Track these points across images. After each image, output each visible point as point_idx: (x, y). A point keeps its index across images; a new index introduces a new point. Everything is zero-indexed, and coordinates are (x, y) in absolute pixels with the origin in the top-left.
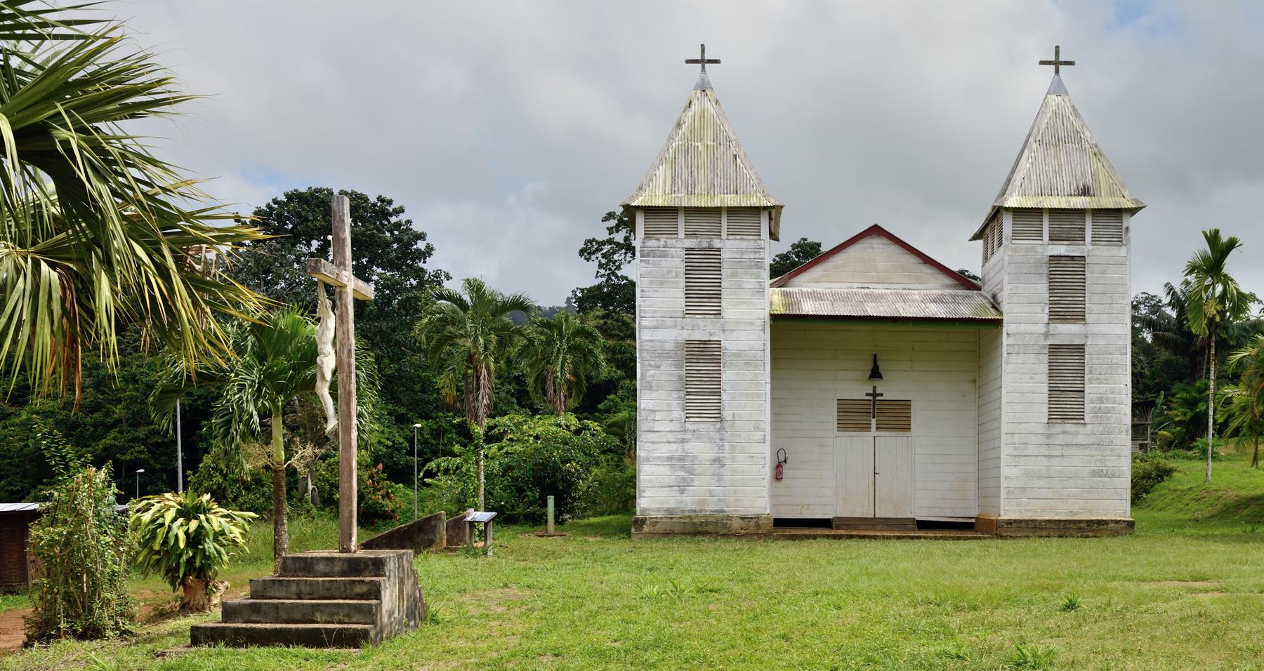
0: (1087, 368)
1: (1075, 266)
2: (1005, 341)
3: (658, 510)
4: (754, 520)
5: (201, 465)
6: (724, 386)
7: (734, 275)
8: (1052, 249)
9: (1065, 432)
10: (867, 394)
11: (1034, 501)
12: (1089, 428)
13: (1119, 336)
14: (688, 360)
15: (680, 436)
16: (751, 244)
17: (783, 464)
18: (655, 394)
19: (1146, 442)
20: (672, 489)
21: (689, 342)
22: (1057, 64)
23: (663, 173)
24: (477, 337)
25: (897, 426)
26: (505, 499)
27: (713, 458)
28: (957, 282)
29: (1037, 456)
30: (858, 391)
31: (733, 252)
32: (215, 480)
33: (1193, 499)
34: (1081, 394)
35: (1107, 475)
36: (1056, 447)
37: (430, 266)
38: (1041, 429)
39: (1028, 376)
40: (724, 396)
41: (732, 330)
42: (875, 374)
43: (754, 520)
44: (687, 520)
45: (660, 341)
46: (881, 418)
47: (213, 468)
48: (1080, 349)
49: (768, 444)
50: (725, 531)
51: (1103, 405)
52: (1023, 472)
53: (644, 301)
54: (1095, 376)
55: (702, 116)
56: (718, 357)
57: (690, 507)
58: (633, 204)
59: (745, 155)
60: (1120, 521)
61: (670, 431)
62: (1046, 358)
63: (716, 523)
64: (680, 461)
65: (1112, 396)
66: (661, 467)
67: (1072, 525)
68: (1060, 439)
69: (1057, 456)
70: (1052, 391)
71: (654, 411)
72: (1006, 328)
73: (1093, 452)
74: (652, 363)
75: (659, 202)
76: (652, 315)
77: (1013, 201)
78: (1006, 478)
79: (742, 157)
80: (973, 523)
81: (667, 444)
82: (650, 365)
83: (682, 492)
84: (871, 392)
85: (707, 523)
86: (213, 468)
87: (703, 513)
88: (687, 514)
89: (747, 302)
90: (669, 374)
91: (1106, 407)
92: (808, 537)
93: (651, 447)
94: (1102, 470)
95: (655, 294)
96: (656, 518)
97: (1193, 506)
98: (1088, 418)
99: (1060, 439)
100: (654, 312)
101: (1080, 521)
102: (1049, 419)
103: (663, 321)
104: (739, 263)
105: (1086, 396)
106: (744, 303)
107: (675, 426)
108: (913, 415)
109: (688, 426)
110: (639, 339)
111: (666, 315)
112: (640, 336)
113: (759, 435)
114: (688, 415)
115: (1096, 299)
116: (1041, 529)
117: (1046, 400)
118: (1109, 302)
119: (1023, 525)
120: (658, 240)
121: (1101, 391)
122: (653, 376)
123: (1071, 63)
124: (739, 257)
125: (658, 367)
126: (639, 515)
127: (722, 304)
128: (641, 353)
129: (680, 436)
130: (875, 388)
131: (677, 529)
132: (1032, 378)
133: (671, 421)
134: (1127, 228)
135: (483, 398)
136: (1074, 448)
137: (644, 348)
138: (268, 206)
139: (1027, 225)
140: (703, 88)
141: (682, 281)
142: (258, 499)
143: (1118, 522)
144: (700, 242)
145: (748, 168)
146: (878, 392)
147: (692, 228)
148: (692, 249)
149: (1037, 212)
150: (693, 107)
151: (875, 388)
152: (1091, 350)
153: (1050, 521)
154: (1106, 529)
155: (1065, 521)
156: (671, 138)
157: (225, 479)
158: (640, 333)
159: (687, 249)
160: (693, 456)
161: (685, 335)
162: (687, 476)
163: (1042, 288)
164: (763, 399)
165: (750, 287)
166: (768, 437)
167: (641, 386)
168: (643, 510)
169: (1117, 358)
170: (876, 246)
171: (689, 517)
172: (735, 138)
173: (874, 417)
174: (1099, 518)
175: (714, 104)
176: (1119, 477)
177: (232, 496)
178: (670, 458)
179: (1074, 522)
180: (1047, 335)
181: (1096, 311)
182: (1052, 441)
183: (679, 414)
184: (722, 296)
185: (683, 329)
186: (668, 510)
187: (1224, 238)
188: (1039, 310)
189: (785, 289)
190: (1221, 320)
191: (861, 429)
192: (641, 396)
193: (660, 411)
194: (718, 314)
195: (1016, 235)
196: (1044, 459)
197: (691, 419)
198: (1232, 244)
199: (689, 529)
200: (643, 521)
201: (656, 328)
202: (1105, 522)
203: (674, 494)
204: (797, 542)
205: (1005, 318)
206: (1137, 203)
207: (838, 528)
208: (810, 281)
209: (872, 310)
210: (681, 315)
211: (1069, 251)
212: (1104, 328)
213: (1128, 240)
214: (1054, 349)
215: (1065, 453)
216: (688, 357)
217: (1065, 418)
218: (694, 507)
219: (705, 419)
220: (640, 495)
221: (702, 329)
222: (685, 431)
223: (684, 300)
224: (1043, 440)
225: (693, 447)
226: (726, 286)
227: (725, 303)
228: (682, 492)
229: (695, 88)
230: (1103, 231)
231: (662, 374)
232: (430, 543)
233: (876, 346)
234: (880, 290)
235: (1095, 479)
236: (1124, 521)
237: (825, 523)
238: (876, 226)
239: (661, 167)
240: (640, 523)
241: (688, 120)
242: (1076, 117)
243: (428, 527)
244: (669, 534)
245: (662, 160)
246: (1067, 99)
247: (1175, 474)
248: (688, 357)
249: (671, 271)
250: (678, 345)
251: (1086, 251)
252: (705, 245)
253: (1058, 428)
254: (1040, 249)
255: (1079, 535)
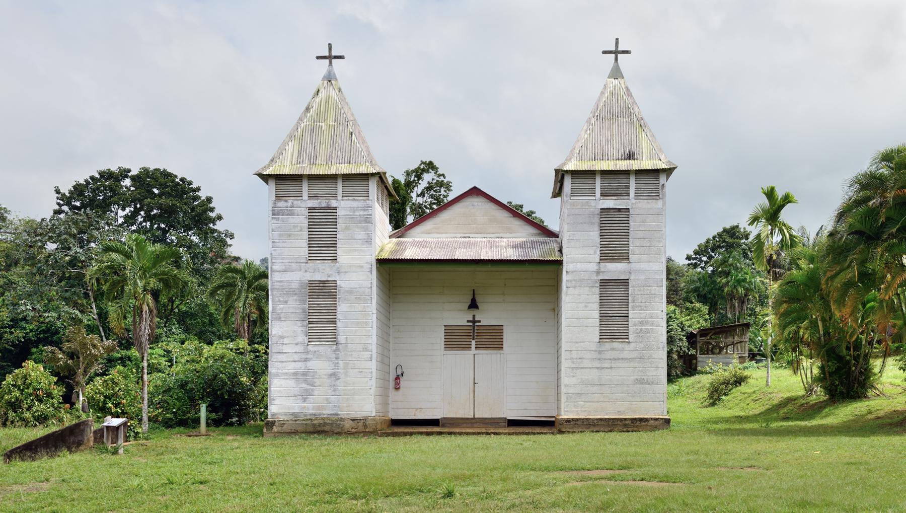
0: (630, 298)
1: (621, 216)
2: (565, 277)
3: (285, 414)
4: (362, 421)
5: (3, 383)
6: (339, 316)
7: (347, 228)
8: (603, 203)
9: (613, 349)
10: (468, 321)
11: (587, 403)
12: (632, 346)
13: (656, 272)
14: (310, 297)
15: (304, 356)
16: (361, 204)
17: (400, 377)
18: (284, 324)
19: (744, 355)
20: (296, 398)
21: (311, 282)
22: (616, 52)
23: (292, 148)
24: (136, 280)
25: (492, 346)
26: (177, 407)
27: (330, 373)
28: (540, 232)
29: (590, 368)
30: (461, 318)
31: (346, 210)
32: (13, 394)
33: (753, 400)
34: (625, 319)
35: (647, 383)
36: (606, 361)
37: (219, 226)
38: (594, 347)
39: (583, 305)
40: (339, 324)
41: (345, 272)
42: (473, 305)
43: (362, 421)
44: (309, 422)
45: (288, 281)
46: (479, 340)
47: (12, 385)
48: (625, 283)
49: (374, 361)
50: (339, 430)
51: (643, 327)
52: (579, 381)
53: (275, 250)
54: (637, 304)
55: (327, 102)
56: (334, 294)
57: (311, 411)
58: (265, 173)
59: (359, 133)
60: (658, 419)
61: (295, 352)
62: (597, 291)
63: (331, 424)
64: (304, 376)
65: (650, 320)
66: (288, 381)
67: (619, 423)
68: (609, 355)
69: (607, 368)
70: (602, 316)
71: (282, 337)
72: (566, 267)
73: (637, 365)
74: (281, 299)
75: (286, 171)
76: (281, 261)
77: (571, 166)
78: (565, 386)
79: (357, 134)
80: (553, 422)
81: (294, 363)
82: (279, 301)
83: (305, 400)
84: (471, 319)
85: (325, 424)
86: (12, 385)
87: (322, 416)
88: (309, 417)
89: (358, 250)
90: (295, 308)
91: (647, 329)
92: (405, 434)
93: (279, 365)
94: (643, 379)
95: (284, 245)
96: (284, 421)
97: (752, 405)
98: (632, 338)
99: (609, 355)
100: (283, 258)
101: (626, 419)
102: (600, 339)
103: (290, 266)
104: (351, 219)
105: (629, 320)
106: (356, 250)
107: (300, 348)
108: (505, 337)
109: (310, 348)
110: (271, 280)
111: (293, 261)
112: (271, 278)
113: (367, 355)
114: (310, 340)
115: (638, 243)
116: (594, 425)
117: (598, 324)
118: (648, 245)
119: (579, 422)
120: (286, 201)
121: (642, 316)
122: (282, 309)
123: (627, 52)
124: (351, 214)
125: (286, 302)
126: (270, 418)
127: (338, 251)
128: (272, 291)
129: (304, 356)
130: (474, 316)
131: (300, 429)
132: (586, 306)
133: (297, 344)
134: (663, 185)
135: (145, 328)
136: (620, 361)
137: (275, 287)
138: (86, 181)
139: (583, 184)
140: (330, 78)
141: (305, 234)
142: (49, 408)
143: (656, 419)
144: (320, 203)
145: (361, 142)
146: (476, 319)
147: (315, 191)
148: (314, 208)
149: (591, 174)
150: (320, 95)
151: (474, 316)
152: (634, 283)
153: (601, 419)
154: (647, 425)
155: (613, 419)
156: (301, 119)
157: (22, 394)
158: (271, 276)
159: (310, 209)
160: (313, 372)
161: (308, 277)
162: (309, 387)
163: (594, 235)
164: (370, 326)
165: (361, 238)
166: (374, 356)
167: (272, 317)
168: (273, 415)
169: (654, 289)
170: (476, 204)
171: (310, 419)
172: (352, 119)
173: (473, 339)
174: (641, 417)
175: (337, 92)
176: (657, 384)
177: (26, 406)
178: (295, 374)
179: (621, 420)
180: (598, 272)
181: (638, 252)
182: (603, 356)
183: (302, 339)
184: (338, 245)
185: (306, 271)
186: (293, 414)
187: (780, 194)
188: (592, 252)
189: (402, 239)
190: (778, 258)
191: (464, 349)
192: (272, 325)
193: (288, 337)
194: (335, 259)
195: (573, 192)
196: (596, 370)
197: (313, 343)
198: (787, 199)
199: (310, 429)
200: (273, 423)
201: (285, 271)
202: (646, 420)
203: (298, 401)
204: (462, 435)
205: (565, 259)
206: (670, 165)
207: (443, 426)
208: (423, 233)
209: (460, 255)
210: (305, 261)
211: (616, 205)
212: (643, 266)
213: (664, 195)
214: (604, 283)
215: (613, 365)
216: (310, 294)
217: (613, 338)
218: (314, 412)
219: (324, 343)
220: (270, 402)
221: (321, 272)
222: (308, 352)
223: (307, 249)
224: (595, 355)
225: (314, 364)
226: (341, 238)
227: (340, 251)
228: (305, 400)
229: (323, 79)
230: (644, 188)
231: (289, 308)
232: (79, 444)
233: (476, 283)
234: (479, 239)
235: (638, 386)
236: (661, 419)
237: (435, 422)
238: (475, 188)
239: (290, 143)
240: (270, 425)
241: (315, 106)
242: (629, 96)
243: (77, 431)
244: (295, 433)
245: (291, 137)
246: (622, 81)
247: (750, 380)
248: (310, 294)
249: (297, 226)
250: (302, 284)
251: (630, 204)
252: (324, 205)
253: (608, 346)
254: (593, 203)
255: (625, 430)
